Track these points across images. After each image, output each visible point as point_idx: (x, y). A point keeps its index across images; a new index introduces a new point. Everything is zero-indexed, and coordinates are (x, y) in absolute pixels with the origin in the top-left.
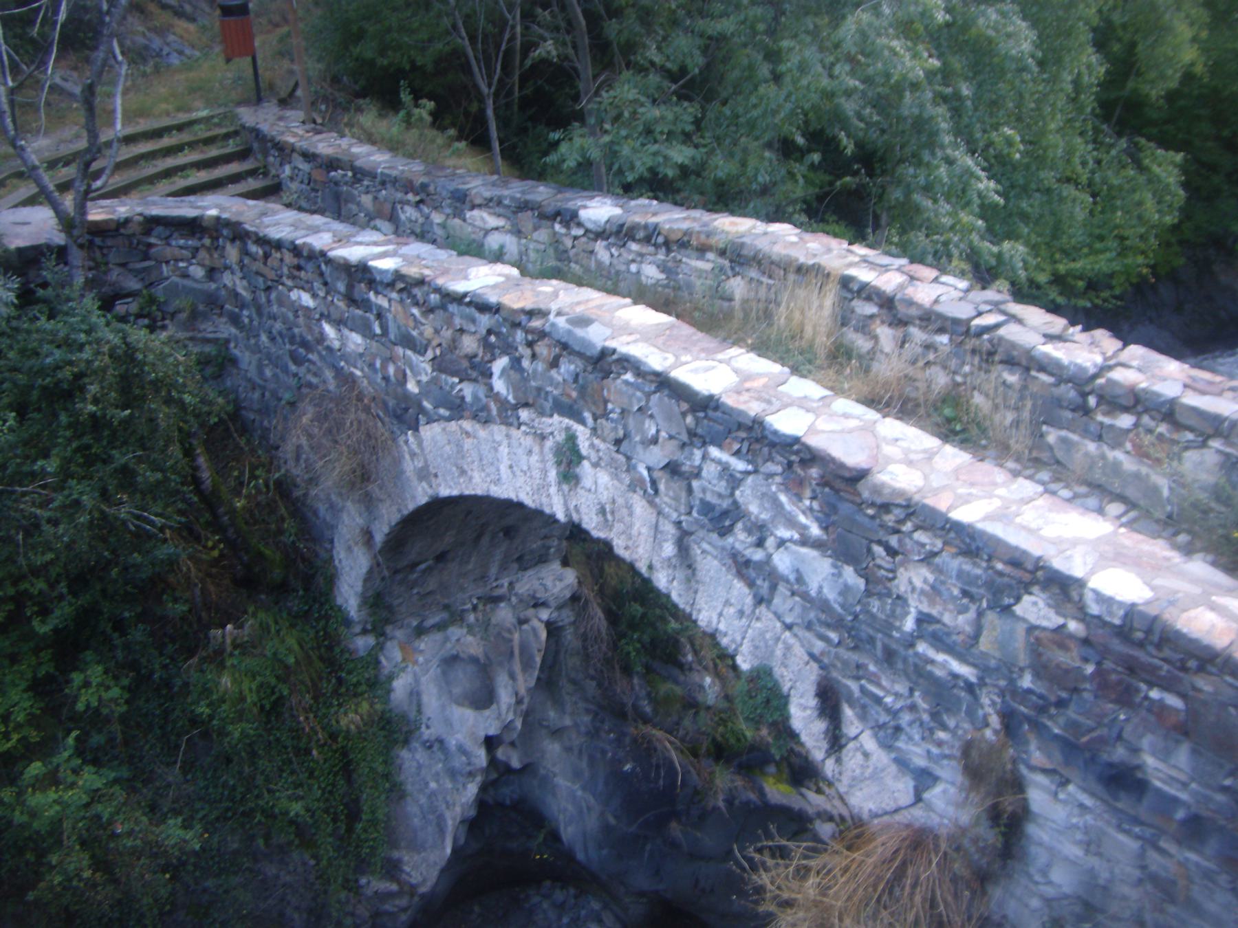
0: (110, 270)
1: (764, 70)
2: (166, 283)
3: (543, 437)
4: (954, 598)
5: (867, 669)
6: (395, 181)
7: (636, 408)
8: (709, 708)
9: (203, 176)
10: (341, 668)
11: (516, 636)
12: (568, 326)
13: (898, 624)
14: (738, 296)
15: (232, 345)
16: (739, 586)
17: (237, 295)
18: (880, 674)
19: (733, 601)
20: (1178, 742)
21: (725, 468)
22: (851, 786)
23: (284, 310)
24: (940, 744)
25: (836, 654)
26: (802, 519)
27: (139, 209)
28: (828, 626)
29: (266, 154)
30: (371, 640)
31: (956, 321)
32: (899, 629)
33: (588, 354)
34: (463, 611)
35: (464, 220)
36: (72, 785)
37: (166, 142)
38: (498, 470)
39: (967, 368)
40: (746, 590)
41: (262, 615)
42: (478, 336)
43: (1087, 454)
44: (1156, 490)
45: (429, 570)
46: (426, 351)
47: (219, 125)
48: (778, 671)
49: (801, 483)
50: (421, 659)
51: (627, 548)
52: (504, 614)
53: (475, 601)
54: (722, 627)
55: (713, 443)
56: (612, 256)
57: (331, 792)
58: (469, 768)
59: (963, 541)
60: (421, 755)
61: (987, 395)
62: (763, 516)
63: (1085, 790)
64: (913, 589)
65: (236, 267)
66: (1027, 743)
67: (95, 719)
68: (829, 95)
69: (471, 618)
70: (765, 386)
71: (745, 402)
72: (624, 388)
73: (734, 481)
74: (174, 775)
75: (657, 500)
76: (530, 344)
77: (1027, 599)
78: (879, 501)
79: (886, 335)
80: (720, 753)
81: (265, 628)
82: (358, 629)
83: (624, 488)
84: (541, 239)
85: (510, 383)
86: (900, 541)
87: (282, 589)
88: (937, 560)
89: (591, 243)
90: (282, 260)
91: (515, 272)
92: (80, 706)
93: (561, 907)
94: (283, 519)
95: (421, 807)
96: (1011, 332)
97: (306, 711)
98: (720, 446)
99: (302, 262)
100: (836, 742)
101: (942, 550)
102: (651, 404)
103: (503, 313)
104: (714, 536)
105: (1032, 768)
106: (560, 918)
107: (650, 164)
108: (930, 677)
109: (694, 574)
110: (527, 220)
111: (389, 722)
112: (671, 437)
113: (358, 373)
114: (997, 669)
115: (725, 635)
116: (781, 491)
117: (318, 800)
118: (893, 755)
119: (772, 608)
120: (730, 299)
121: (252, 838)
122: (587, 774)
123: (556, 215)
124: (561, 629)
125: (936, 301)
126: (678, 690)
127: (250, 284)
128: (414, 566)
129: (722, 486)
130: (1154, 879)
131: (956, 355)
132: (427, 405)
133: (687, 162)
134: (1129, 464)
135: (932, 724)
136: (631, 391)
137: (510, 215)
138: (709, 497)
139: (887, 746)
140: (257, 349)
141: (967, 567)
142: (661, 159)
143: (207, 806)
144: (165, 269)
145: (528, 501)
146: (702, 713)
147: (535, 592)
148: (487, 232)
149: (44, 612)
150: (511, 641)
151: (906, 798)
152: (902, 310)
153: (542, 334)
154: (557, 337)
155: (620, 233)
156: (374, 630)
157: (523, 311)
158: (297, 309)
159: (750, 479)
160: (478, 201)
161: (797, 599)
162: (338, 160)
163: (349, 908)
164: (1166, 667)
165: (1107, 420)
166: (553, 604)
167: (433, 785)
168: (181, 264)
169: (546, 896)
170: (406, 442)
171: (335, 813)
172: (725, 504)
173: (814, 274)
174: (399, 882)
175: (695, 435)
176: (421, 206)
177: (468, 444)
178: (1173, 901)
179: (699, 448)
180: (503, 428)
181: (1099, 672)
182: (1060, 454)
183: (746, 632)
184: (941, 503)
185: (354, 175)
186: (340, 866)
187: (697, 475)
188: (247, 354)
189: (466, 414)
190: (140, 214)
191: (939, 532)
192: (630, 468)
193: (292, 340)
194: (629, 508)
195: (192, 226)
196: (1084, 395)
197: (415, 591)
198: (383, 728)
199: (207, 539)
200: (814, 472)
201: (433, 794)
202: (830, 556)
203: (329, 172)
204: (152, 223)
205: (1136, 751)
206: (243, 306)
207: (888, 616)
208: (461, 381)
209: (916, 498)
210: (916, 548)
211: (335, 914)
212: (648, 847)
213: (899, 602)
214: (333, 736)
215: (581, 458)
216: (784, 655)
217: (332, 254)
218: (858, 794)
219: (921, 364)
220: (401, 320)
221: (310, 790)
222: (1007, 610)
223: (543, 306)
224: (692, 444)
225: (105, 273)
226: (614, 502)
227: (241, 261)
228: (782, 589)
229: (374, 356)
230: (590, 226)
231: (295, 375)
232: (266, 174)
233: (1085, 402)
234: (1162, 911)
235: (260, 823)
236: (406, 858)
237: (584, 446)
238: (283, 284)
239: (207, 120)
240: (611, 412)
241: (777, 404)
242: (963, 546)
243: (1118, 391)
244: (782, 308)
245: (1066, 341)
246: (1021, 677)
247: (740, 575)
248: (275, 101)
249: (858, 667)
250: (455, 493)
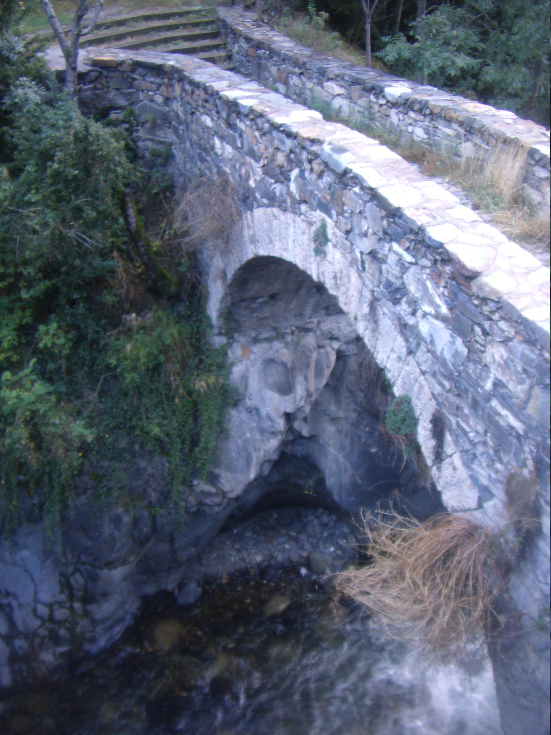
0: (110, 91)
2: (141, 104)
4: (517, 372)
5: (462, 411)
7: (358, 211)
9: (187, 45)
10: (203, 353)
11: (315, 355)
12: (330, 152)
13: (482, 383)
15: (173, 147)
16: (400, 340)
17: (178, 116)
18: (470, 416)
19: (396, 349)
23: (198, 127)
24: (497, 472)
25: (447, 397)
26: (438, 300)
27: (131, 56)
28: (445, 377)
29: (227, 36)
32: (482, 387)
33: (337, 171)
34: (285, 333)
35: (323, 88)
36: (29, 390)
37: (171, 22)
38: (287, 242)
40: (404, 344)
41: (160, 313)
42: (285, 154)
45: (264, 303)
46: (260, 160)
47: (205, 16)
49: (440, 275)
50: (252, 357)
51: (346, 304)
52: (310, 340)
53: (294, 329)
54: (388, 366)
56: (399, 120)
57: (183, 426)
58: (273, 430)
59: (527, 333)
60: (244, 415)
62: (416, 295)
64: (494, 361)
65: (179, 98)
69: (289, 338)
70: (438, 208)
71: (419, 216)
72: (353, 196)
74: (94, 396)
75: (363, 275)
76: (310, 161)
78: (481, 295)
81: (159, 319)
82: (216, 331)
83: (347, 264)
84: (362, 104)
86: (491, 326)
87: (175, 299)
88: (510, 344)
89: (389, 110)
91: (318, 115)
92: (41, 345)
93: (324, 526)
98: (399, 243)
101: (514, 337)
102: (367, 209)
103: (298, 139)
106: (322, 532)
108: (496, 425)
110: (357, 89)
111: (226, 391)
112: (374, 233)
114: (537, 428)
115: (390, 371)
116: (428, 279)
117: (175, 429)
118: (470, 473)
121: (133, 443)
122: (348, 449)
127: (184, 109)
128: (254, 299)
129: (396, 271)
132: (258, 195)
133: (465, 67)
135: (495, 458)
139: (467, 465)
140: (184, 151)
141: (527, 352)
142: (449, 63)
143: (110, 420)
144: (141, 94)
147: (333, 330)
148: (335, 96)
149: (29, 287)
150: (309, 357)
151: (473, 504)
153: (317, 156)
160: (331, 76)
161: (429, 355)
162: (263, 43)
166: (343, 339)
168: (151, 93)
169: (318, 517)
170: (247, 218)
171: (184, 439)
172: (398, 283)
173: (513, 145)
176: (302, 77)
177: (275, 223)
179: (388, 243)
180: (292, 215)
183: (400, 372)
185: (269, 54)
186: (182, 471)
188: (180, 153)
189: (276, 204)
190: (130, 59)
191: (514, 324)
192: (352, 251)
194: (349, 277)
197: (255, 315)
198: (222, 395)
200: (448, 269)
201: (246, 441)
202: (450, 329)
203: (257, 50)
204: (137, 65)
206: (180, 123)
207: (478, 377)
208: (276, 182)
209: (505, 297)
210: (499, 332)
211: (174, 498)
213: (485, 369)
214: (190, 393)
215: (327, 240)
216: (419, 391)
217: (222, 93)
218: (448, 493)
221: (171, 422)
223: (321, 138)
224: (384, 239)
225: (107, 93)
226: (342, 272)
227: (181, 95)
228: (423, 347)
229: (236, 161)
230: (389, 98)
231: (200, 169)
236: (223, 475)
237: (330, 232)
238: (199, 111)
239: (198, 12)
241: (439, 219)
242: (527, 337)
247: (402, 333)
248: (243, 6)
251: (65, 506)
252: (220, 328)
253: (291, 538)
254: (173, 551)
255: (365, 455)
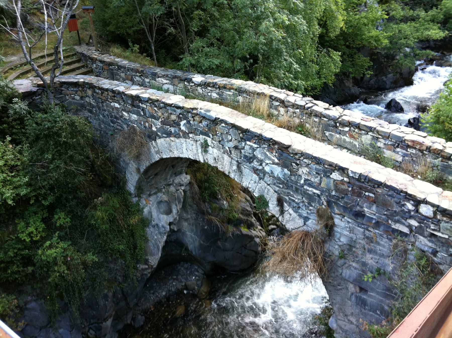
1: (237, 37)
3: (197, 141)
6: (132, 70)
8: (226, 210)
14: (240, 101)
15: (89, 118)
16: (255, 176)
17: (91, 104)
20: (373, 205)
21: (251, 146)
22: (286, 223)
24: (310, 210)
26: (273, 158)
28: (280, 184)
30: (137, 199)
31: (301, 106)
32: (300, 183)
35: (156, 81)
36: (57, 248)
39: (304, 118)
40: (257, 176)
43: (336, 138)
44: (355, 145)
45: (153, 178)
48: (266, 196)
49: (273, 149)
50: (151, 203)
52: (172, 189)
54: (250, 186)
55: (248, 140)
60: (152, 229)
61: (310, 124)
63: (349, 218)
64: (303, 173)
66: (334, 208)
67: (61, 228)
68: (257, 44)
69: (164, 190)
72: (222, 128)
73: (254, 150)
74: (84, 242)
76: (193, 117)
77: (333, 173)
78: (294, 153)
79: (282, 110)
80: (229, 221)
82: (134, 196)
85: (186, 127)
87: (111, 186)
88: (310, 166)
90: (108, 94)
92: (58, 225)
94: (110, 167)
95: (153, 244)
96: (315, 108)
97: (121, 220)
98: (250, 141)
99: (115, 95)
100: (282, 212)
104: (248, 163)
105: (335, 214)
107: (209, 65)
109: (242, 173)
110: (176, 81)
112: (236, 140)
113: (136, 126)
114: (326, 191)
115: (251, 188)
119: (264, 180)
120: (239, 102)
121: (107, 257)
123: (186, 80)
124: (187, 191)
125: (295, 101)
126: (218, 206)
128: (149, 177)
129: (250, 151)
130: (367, 238)
131: (301, 115)
134: (348, 139)
136: (224, 128)
137: (170, 79)
138: (246, 154)
139: (296, 212)
141: (318, 167)
145: (192, 158)
146: (224, 211)
148: (163, 84)
152: (286, 103)
153: (197, 114)
154: (201, 115)
155: (205, 85)
156: (138, 196)
157: (191, 108)
158: (113, 108)
159: (258, 149)
160: (160, 76)
163: (135, 274)
164: (369, 187)
165: (342, 129)
166: (185, 185)
167: (156, 237)
169: (182, 266)
170: (152, 144)
174: (148, 265)
175: (243, 139)
177: (173, 144)
178: (372, 242)
181: (353, 189)
182: (329, 138)
184: (310, 152)
185: (118, 68)
187: (243, 148)
188: (95, 121)
193: (112, 117)
195: (76, 85)
196: (336, 123)
198: (142, 223)
199: (88, 174)
200: (276, 146)
201: (156, 239)
205: (362, 207)
209: (304, 151)
212: (212, 249)
214: (129, 226)
216: (268, 192)
217: (126, 93)
218: (288, 224)
219: (292, 116)
220: (151, 111)
222: (329, 177)
224: (242, 141)
227: (93, 94)
230: (196, 83)
232: (87, 67)
233: (336, 125)
234: (370, 245)
235: (109, 253)
240: (218, 134)
243: (345, 122)
244: (254, 103)
245: (330, 110)
246: (332, 192)
247: (255, 173)
249: (288, 193)
250: (168, 157)
251: (81, 298)
252: (135, 194)
253: (174, 279)
254: (127, 304)
255: (203, 230)
